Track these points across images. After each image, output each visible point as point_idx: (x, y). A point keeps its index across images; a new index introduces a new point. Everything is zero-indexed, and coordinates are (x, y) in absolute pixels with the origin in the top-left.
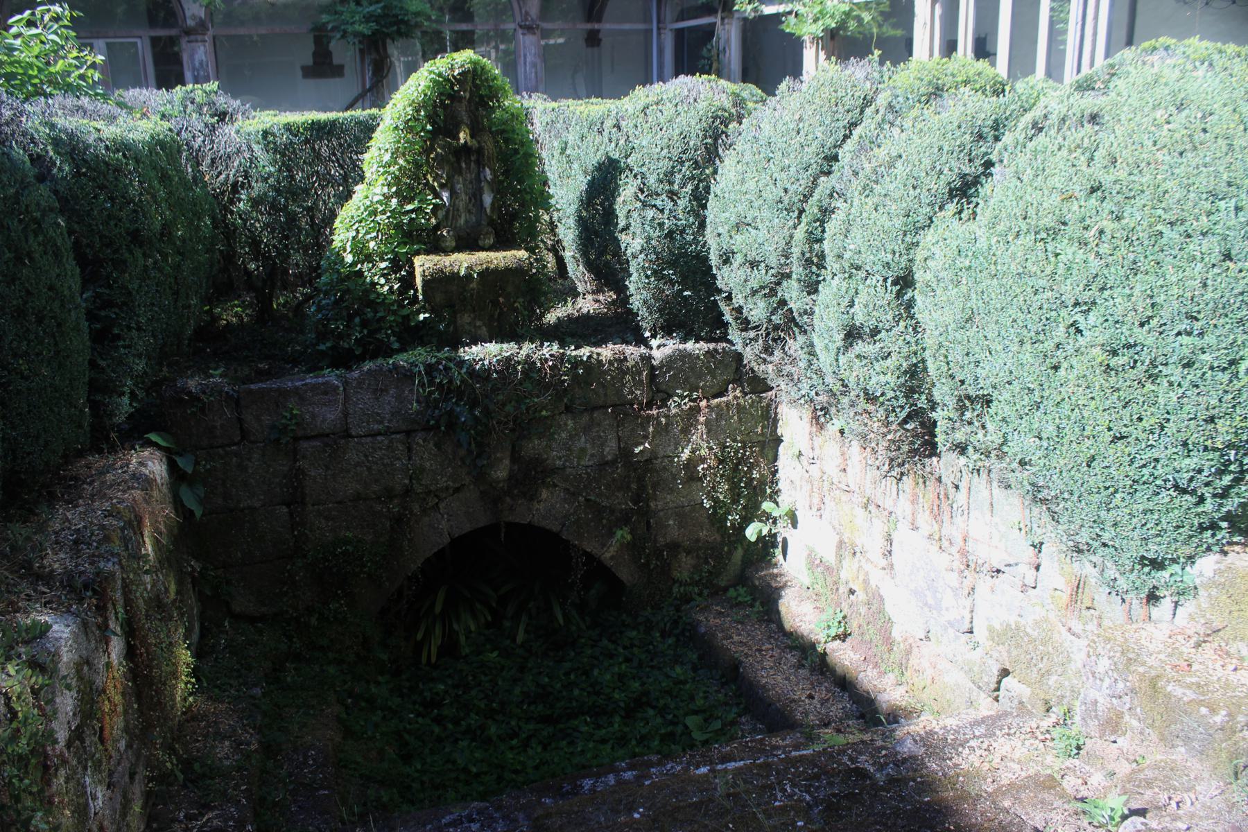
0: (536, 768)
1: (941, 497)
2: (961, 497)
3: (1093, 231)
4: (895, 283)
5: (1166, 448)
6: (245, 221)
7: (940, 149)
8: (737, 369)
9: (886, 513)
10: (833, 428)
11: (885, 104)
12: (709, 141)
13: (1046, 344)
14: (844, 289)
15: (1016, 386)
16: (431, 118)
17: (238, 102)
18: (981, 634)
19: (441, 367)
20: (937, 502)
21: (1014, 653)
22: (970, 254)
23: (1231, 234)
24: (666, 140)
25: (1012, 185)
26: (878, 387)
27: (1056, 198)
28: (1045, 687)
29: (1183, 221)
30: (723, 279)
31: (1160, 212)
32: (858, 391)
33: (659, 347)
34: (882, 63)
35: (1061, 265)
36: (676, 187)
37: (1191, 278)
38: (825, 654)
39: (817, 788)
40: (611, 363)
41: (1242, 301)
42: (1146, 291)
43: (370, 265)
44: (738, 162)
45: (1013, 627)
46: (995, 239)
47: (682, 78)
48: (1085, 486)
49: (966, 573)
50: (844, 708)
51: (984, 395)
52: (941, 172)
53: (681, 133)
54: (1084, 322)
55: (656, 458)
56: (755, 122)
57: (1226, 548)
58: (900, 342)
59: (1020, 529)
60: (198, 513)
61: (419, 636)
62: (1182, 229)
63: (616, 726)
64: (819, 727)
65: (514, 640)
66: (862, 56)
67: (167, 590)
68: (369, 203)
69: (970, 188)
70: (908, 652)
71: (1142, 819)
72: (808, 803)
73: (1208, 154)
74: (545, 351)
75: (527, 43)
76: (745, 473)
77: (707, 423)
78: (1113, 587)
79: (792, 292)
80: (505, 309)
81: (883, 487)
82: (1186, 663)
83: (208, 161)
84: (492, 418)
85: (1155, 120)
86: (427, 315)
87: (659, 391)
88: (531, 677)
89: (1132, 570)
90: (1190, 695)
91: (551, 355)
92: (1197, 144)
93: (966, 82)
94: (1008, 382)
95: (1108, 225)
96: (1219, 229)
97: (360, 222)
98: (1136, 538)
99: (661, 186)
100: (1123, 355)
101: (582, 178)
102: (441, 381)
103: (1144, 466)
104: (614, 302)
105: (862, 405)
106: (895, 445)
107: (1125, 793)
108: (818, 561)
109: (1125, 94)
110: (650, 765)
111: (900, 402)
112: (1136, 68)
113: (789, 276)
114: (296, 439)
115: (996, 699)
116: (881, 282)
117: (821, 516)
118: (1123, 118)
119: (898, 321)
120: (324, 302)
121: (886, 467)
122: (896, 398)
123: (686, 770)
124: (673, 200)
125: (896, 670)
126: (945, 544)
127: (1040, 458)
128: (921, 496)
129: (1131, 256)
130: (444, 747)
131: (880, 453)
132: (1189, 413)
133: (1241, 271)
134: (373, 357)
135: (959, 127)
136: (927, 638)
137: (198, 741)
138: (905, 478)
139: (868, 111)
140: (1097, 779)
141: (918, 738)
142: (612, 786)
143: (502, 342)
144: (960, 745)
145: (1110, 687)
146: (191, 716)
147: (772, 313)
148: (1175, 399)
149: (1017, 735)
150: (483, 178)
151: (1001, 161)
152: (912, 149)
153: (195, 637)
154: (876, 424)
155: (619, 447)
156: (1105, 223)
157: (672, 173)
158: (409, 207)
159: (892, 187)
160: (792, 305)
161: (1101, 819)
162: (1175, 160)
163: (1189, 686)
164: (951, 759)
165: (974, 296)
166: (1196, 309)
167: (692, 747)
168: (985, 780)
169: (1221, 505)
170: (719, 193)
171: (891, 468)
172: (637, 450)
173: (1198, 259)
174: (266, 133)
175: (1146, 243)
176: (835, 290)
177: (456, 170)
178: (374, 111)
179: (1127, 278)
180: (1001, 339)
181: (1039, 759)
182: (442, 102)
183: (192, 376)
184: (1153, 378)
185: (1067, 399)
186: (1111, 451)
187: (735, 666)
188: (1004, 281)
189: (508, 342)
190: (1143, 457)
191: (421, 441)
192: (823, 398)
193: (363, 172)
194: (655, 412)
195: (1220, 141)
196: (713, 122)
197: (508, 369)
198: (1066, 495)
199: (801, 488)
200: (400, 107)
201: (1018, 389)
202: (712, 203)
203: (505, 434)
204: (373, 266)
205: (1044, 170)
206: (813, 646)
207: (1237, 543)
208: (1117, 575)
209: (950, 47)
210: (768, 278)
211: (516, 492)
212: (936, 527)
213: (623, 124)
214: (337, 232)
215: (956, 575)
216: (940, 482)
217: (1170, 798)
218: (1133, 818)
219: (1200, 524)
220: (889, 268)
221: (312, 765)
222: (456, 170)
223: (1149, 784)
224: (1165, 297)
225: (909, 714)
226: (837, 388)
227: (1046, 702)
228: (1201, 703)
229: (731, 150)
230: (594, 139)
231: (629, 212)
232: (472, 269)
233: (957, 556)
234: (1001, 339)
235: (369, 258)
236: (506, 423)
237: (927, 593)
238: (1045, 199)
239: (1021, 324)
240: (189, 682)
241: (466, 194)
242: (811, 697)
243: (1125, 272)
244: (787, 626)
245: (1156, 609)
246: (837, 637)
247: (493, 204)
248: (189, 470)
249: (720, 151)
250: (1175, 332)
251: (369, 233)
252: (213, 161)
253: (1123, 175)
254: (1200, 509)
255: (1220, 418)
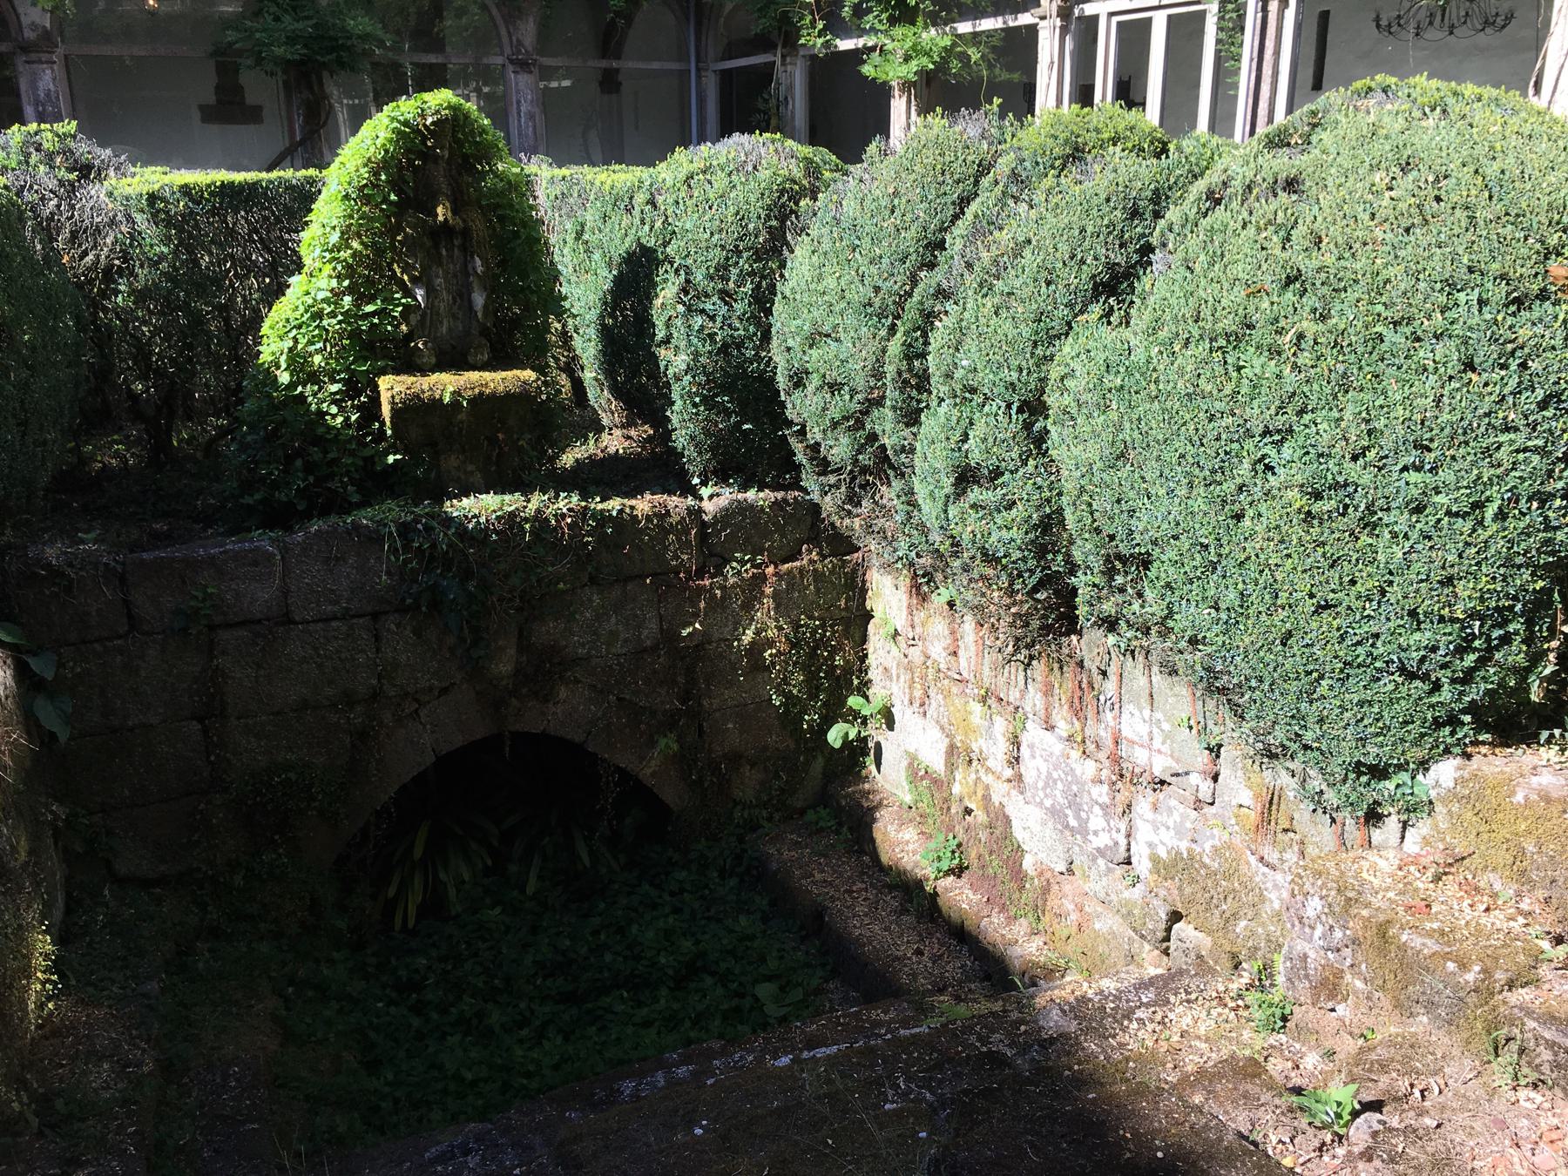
0: (556, 1067)
1: (1084, 685)
2: (1110, 687)
3: (1290, 336)
4: (1020, 411)
5: (1388, 619)
6: (125, 322)
7: (1083, 230)
8: (813, 525)
9: (1011, 708)
10: (940, 598)
11: (1007, 171)
12: (774, 223)
13: (1225, 486)
14: (954, 419)
15: (1185, 543)
16: (394, 184)
17: (108, 152)
18: (1142, 865)
19: (419, 526)
20: (1080, 694)
21: (1188, 890)
22: (1122, 370)
23: (1474, 336)
24: (718, 223)
25: (1177, 277)
26: (1000, 545)
27: (1239, 293)
28: (1231, 936)
29: (1410, 320)
30: (794, 408)
31: (1380, 308)
32: (973, 552)
33: (711, 497)
34: (1002, 116)
35: (1245, 381)
36: (731, 285)
37: (1421, 396)
38: (936, 894)
39: (940, 1082)
40: (648, 518)
41: (1489, 424)
42: (1360, 413)
43: (316, 388)
44: (813, 252)
45: (1185, 856)
46: (1156, 350)
47: (736, 137)
48: (1279, 670)
49: (1119, 785)
50: (962, 966)
51: (1140, 554)
52: (1083, 262)
53: (737, 213)
54: (1276, 456)
55: (710, 643)
56: (835, 197)
57: (1469, 750)
58: (1029, 487)
59: (1191, 728)
60: (63, 736)
61: (392, 892)
62: (1408, 330)
63: (663, 1001)
64: (932, 993)
65: (523, 891)
66: (976, 106)
67: (14, 849)
68: (310, 302)
69: (1122, 283)
70: (1046, 890)
71: (1378, 1116)
72: (931, 1105)
73: (1444, 229)
74: (561, 504)
75: (522, 86)
76: (826, 659)
77: (776, 596)
78: (1319, 802)
79: (885, 424)
80: (506, 449)
81: (1006, 674)
82: (1424, 903)
83: (66, 234)
84: (492, 594)
85: (1373, 185)
86: (398, 457)
87: (712, 555)
88: (547, 941)
89: (1345, 781)
90: (1432, 946)
91: (569, 510)
92: (1429, 217)
93: (1115, 141)
94: (1173, 537)
95: (1310, 327)
96: (1458, 329)
97: (300, 327)
98: (1349, 737)
99: (712, 284)
100: (1330, 498)
101: (605, 273)
102: (421, 545)
103: (1359, 643)
104: (650, 439)
105: (980, 568)
106: (1023, 619)
107: (1353, 1081)
108: (922, 772)
109: (1333, 150)
110: (710, 1055)
111: (1029, 564)
112: (1347, 115)
113: (879, 402)
114: (212, 628)
115: (1166, 952)
116: (1003, 409)
117: (925, 714)
118: (1330, 183)
119: (1027, 460)
120: (249, 438)
121: (1010, 648)
122: (1024, 559)
123: (760, 1060)
124: (726, 303)
125: (1030, 915)
126: (1091, 747)
127: (1217, 635)
128: (1057, 686)
129: (1341, 368)
130: (427, 1046)
131: (1001, 630)
132: (1418, 573)
133: (1486, 384)
134: (324, 513)
135: (1108, 200)
136: (1070, 871)
137: (62, 1066)
138: (1034, 663)
139: (985, 182)
140: (1311, 1061)
141: (1066, 1008)
142: (661, 1089)
143: (504, 493)
144: (1124, 1017)
145: (1323, 937)
146: (52, 1030)
147: (859, 452)
148: (1400, 555)
149: (1200, 1003)
150: (471, 271)
151: (1164, 245)
152: (1044, 232)
153: (58, 914)
154: (996, 594)
155: (661, 628)
156: (1305, 324)
157: (726, 268)
158: (370, 308)
159: (1017, 283)
160: (886, 441)
161: (1325, 1118)
162: (1400, 238)
163: (1430, 934)
164: (1114, 1037)
165: (1127, 425)
166: (1428, 436)
167: (765, 1026)
168: (1164, 1065)
169: (1461, 693)
170: (788, 294)
171: (1017, 650)
172: (685, 633)
173: (1431, 370)
174: (153, 198)
175: (1360, 350)
176: (943, 420)
177: (433, 259)
178: (312, 172)
179: (1335, 397)
180: (1163, 480)
181: (1234, 1035)
182: (410, 162)
183: (52, 542)
184: (1371, 526)
185: (1253, 558)
186: (1314, 625)
187: (819, 914)
188: (1169, 404)
189: (512, 492)
190: (1357, 631)
191: (393, 627)
192: (926, 561)
193: (300, 258)
194: (707, 583)
195: (1458, 212)
196: (779, 198)
197: (511, 528)
198: (1253, 683)
199: (898, 677)
200: (351, 167)
201: (1187, 546)
202: (778, 307)
203: (508, 614)
204: (320, 389)
205: (1222, 255)
206: (919, 884)
207: (1483, 743)
208: (1324, 787)
209: (1084, 95)
210: (854, 406)
211: (524, 691)
212: (1077, 725)
213: (660, 199)
214: (265, 340)
215: (1105, 788)
216: (1082, 667)
217: (1412, 1086)
218: (1367, 1114)
219: (1435, 719)
220: (1014, 390)
221: (235, 1088)
222: (433, 259)
223: (1384, 1067)
224: (1387, 421)
225: (1051, 973)
226: (945, 548)
227: (1234, 956)
228: (1447, 957)
229: (804, 236)
230: (621, 220)
231: (670, 319)
232: (460, 395)
233: (1107, 763)
234: (1163, 480)
235: (313, 377)
236: (510, 600)
237: (1068, 812)
238: (1225, 294)
239: (1191, 460)
240: (48, 981)
241: (449, 292)
242: (919, 952)
243: (1332, 389)
244: (884, 859)
245: (1378, 831)
246: (950, 872)
247: (485, 307)
248: (49, 675)
249: (789, 237)
250: (1400, 466)
251: (313, 344)
252: (74, 235)
253: (1329, 259)
254: (1434, 700)
255: (1460, 579)
